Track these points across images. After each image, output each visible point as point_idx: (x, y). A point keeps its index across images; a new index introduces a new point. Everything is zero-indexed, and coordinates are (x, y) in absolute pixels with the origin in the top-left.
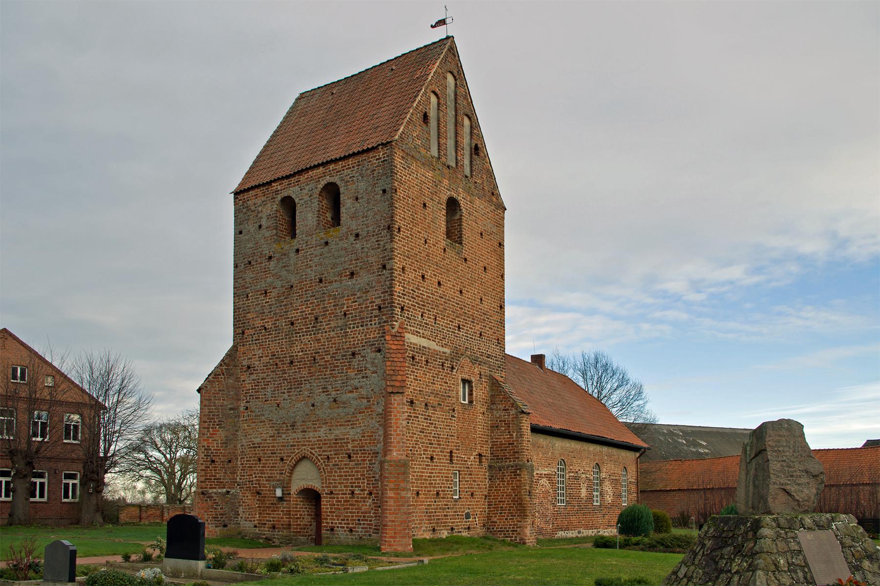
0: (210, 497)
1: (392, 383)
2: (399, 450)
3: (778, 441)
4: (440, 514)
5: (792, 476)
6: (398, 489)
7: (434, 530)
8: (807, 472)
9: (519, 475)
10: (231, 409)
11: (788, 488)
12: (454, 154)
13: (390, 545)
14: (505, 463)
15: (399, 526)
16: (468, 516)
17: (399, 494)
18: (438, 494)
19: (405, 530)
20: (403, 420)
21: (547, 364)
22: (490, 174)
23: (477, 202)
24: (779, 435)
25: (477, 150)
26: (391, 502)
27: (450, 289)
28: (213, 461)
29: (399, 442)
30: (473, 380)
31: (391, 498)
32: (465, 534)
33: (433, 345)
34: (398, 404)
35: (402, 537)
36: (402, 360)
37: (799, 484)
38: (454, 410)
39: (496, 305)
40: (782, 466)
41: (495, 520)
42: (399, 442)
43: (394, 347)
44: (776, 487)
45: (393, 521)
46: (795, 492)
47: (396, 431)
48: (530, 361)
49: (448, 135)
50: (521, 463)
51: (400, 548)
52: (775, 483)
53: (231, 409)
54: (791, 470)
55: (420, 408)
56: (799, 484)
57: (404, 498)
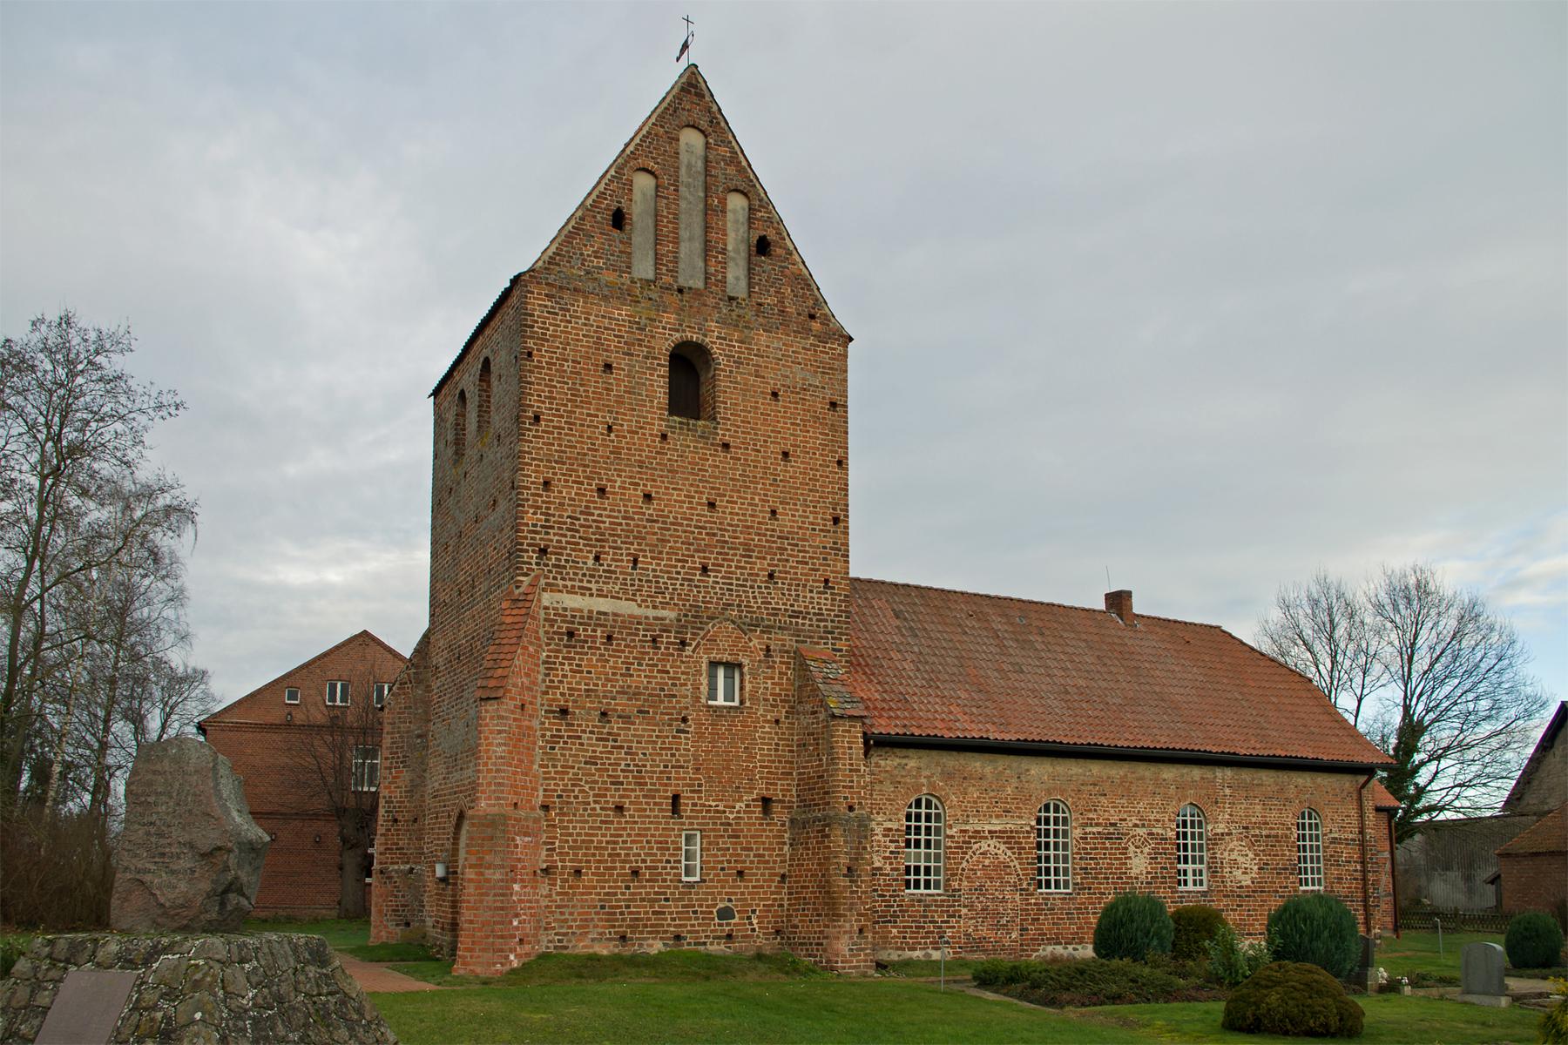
0: (390, 878)
1: (485, 683)
2: (489, 798)
3: (150, 784)
4: (644, 911)
5: (163, 855)
6: (480, 866)
7: (623, 938)
8: (192, 847)
9: (828, 836)
10: (419, 736)
11: (148, 878)
12: (701, 264)
13: (464, 964)
14: (812, 814)
15: (480, 930)
16: (726, 914)
17: (482, 874)
18: (635, 873)
19: (488, 937)
20: (500, 745)
21: (1138, 607)
22: (805, 283)
23: (763, 338)
24: (155, 772)
25: (767, 244)
26: (471, 889)
27: (678, 501)
28: (396, 821)
29: (489, 784)
30: (746, 661)
31: (470, 880)
32: (716, 948)
33: (627, 608)
34: (492, 718)
35: (483, 950)
36: (514, 641)
37: (173, 872)
38: (685, 720)
39: (822, 518)
40: (148, 834)
41: (796, 922)
42: (489, 784)
43: (509, 620)
44: (128, 876)
45: (471, 922)
46: (159, 888)
47: (486, 764)
48: (1101, 606)
49: (684, 234)
50: (832, 813)
51: (478, 970)
52: (126, 869)
53: (419, 736)
54: (162, 841)
55: (585, 720)
56: (173, 872)
57: (488, 881)
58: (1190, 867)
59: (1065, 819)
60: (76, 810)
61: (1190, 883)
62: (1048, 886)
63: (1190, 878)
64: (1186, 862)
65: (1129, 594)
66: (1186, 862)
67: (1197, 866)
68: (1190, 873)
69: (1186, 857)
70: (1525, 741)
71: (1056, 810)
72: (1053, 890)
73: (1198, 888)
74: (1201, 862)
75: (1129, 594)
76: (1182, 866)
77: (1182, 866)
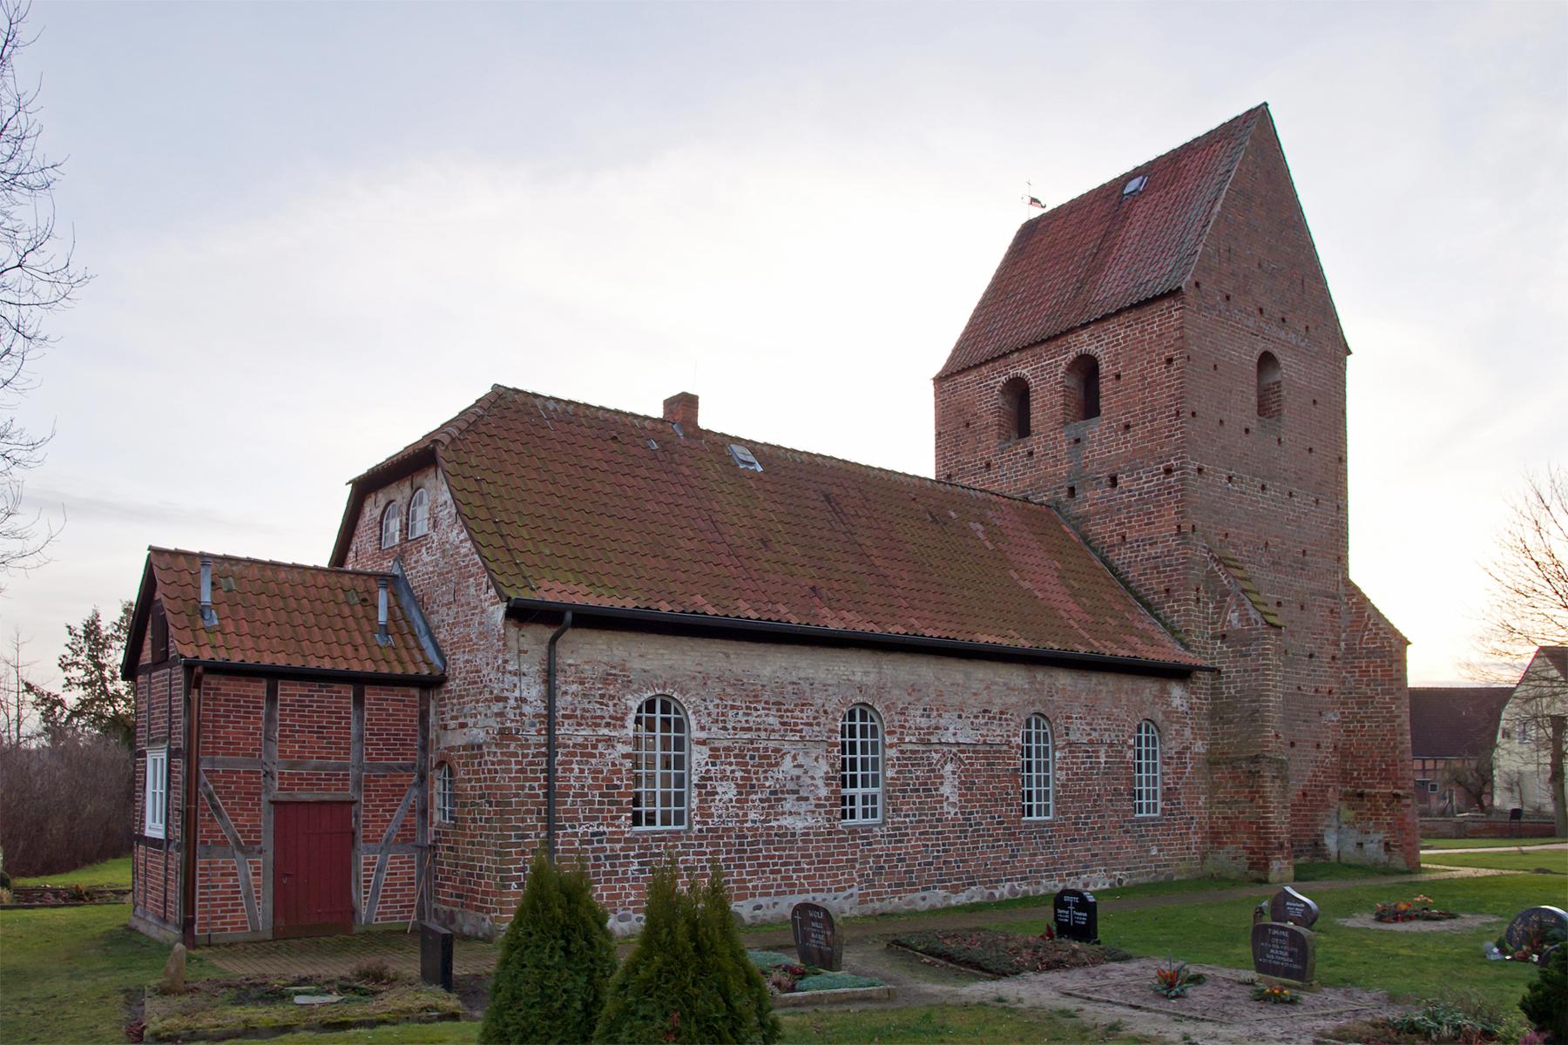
58: (859, 791)
59: (874, 728)
60: (34, 746)
61: (859, 813)
62: (651, 822)
63: (859, 807)
64: (854, 785)
65: (1266, 104)
66: (854, 785)
67: (870, 790)
68: (859, 800)
69: (854, 778)
70: (1122, 644)
71: (864, 717)
72: (658, 827)
73: (870, 820)
74: (875, 785)
75: (1266, 104)
76: (848, 791)
77: (848, 791)
